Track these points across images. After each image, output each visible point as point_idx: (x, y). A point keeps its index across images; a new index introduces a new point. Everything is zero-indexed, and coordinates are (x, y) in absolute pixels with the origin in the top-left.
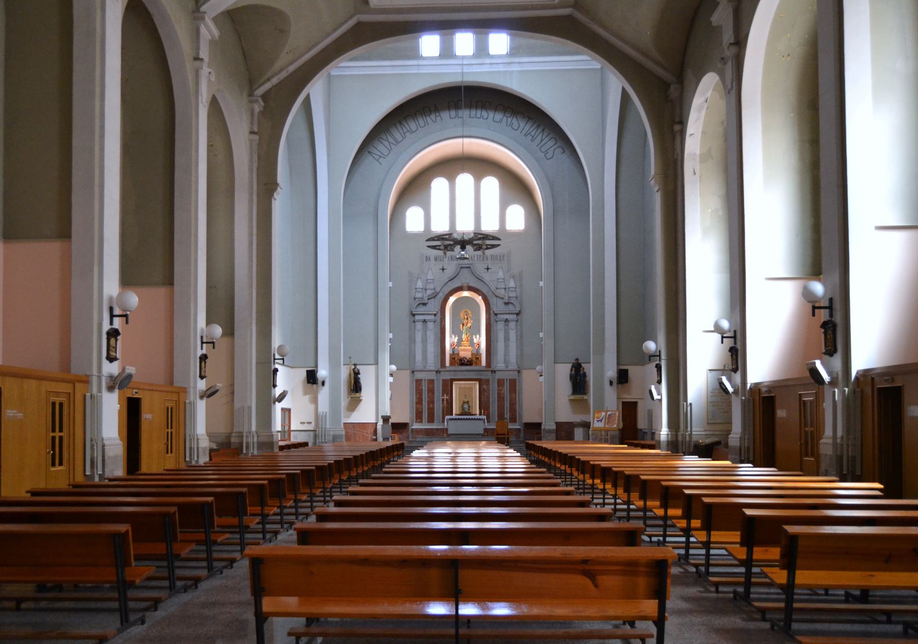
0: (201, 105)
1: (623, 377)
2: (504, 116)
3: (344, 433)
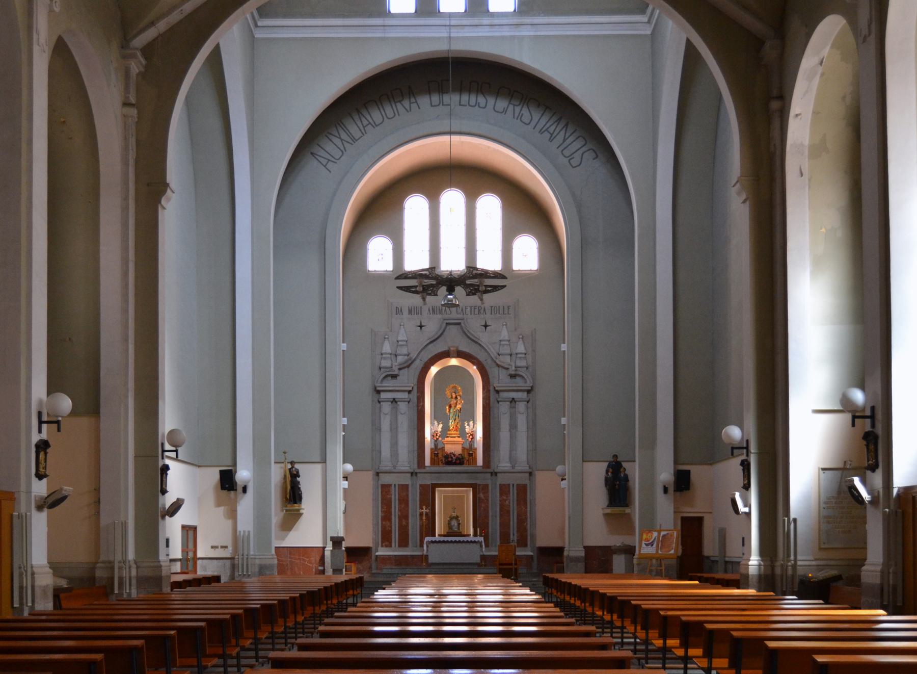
0: (36, 48)
1: (682, 481)
2: (510, 103)
3: (276, 562)
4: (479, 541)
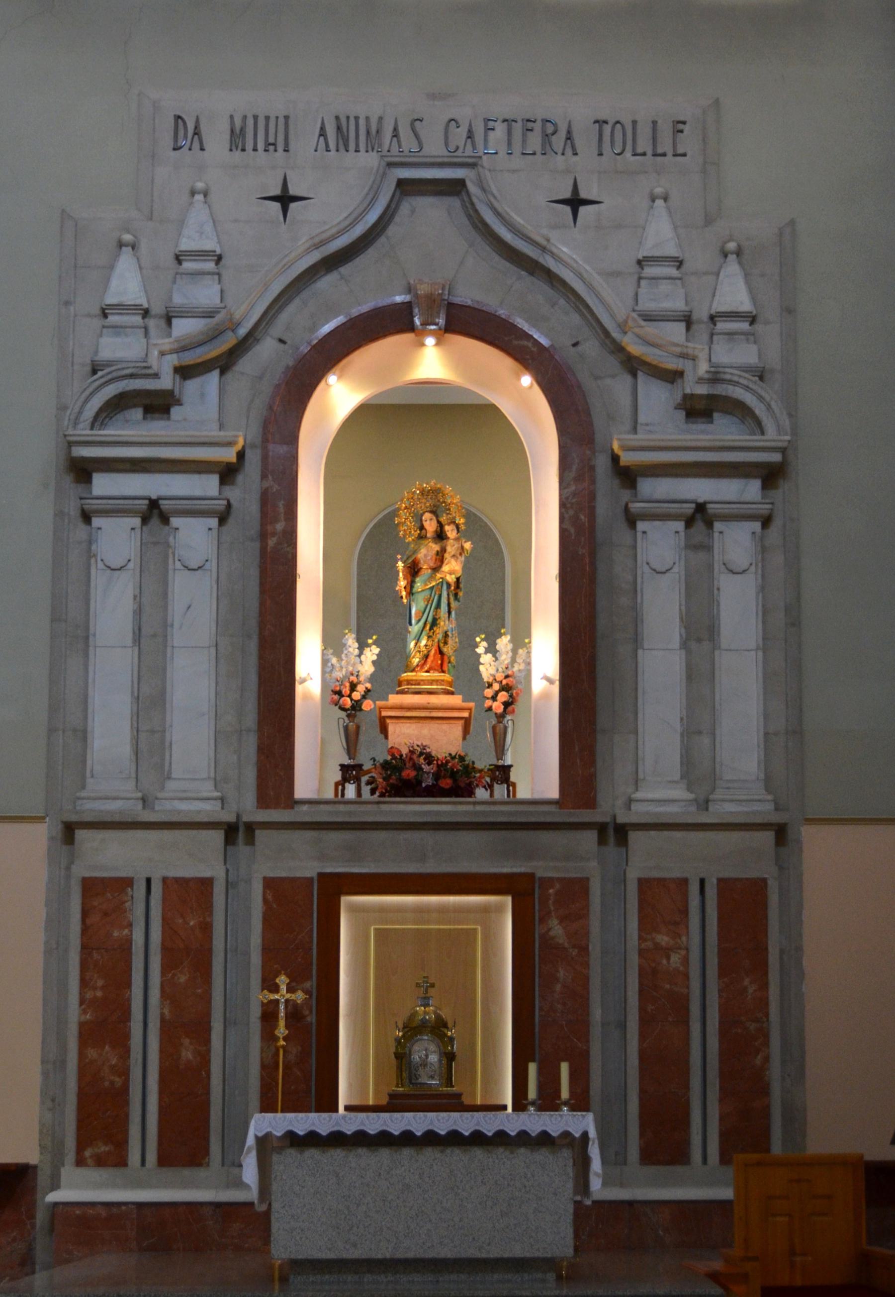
4: (566, 1134)
